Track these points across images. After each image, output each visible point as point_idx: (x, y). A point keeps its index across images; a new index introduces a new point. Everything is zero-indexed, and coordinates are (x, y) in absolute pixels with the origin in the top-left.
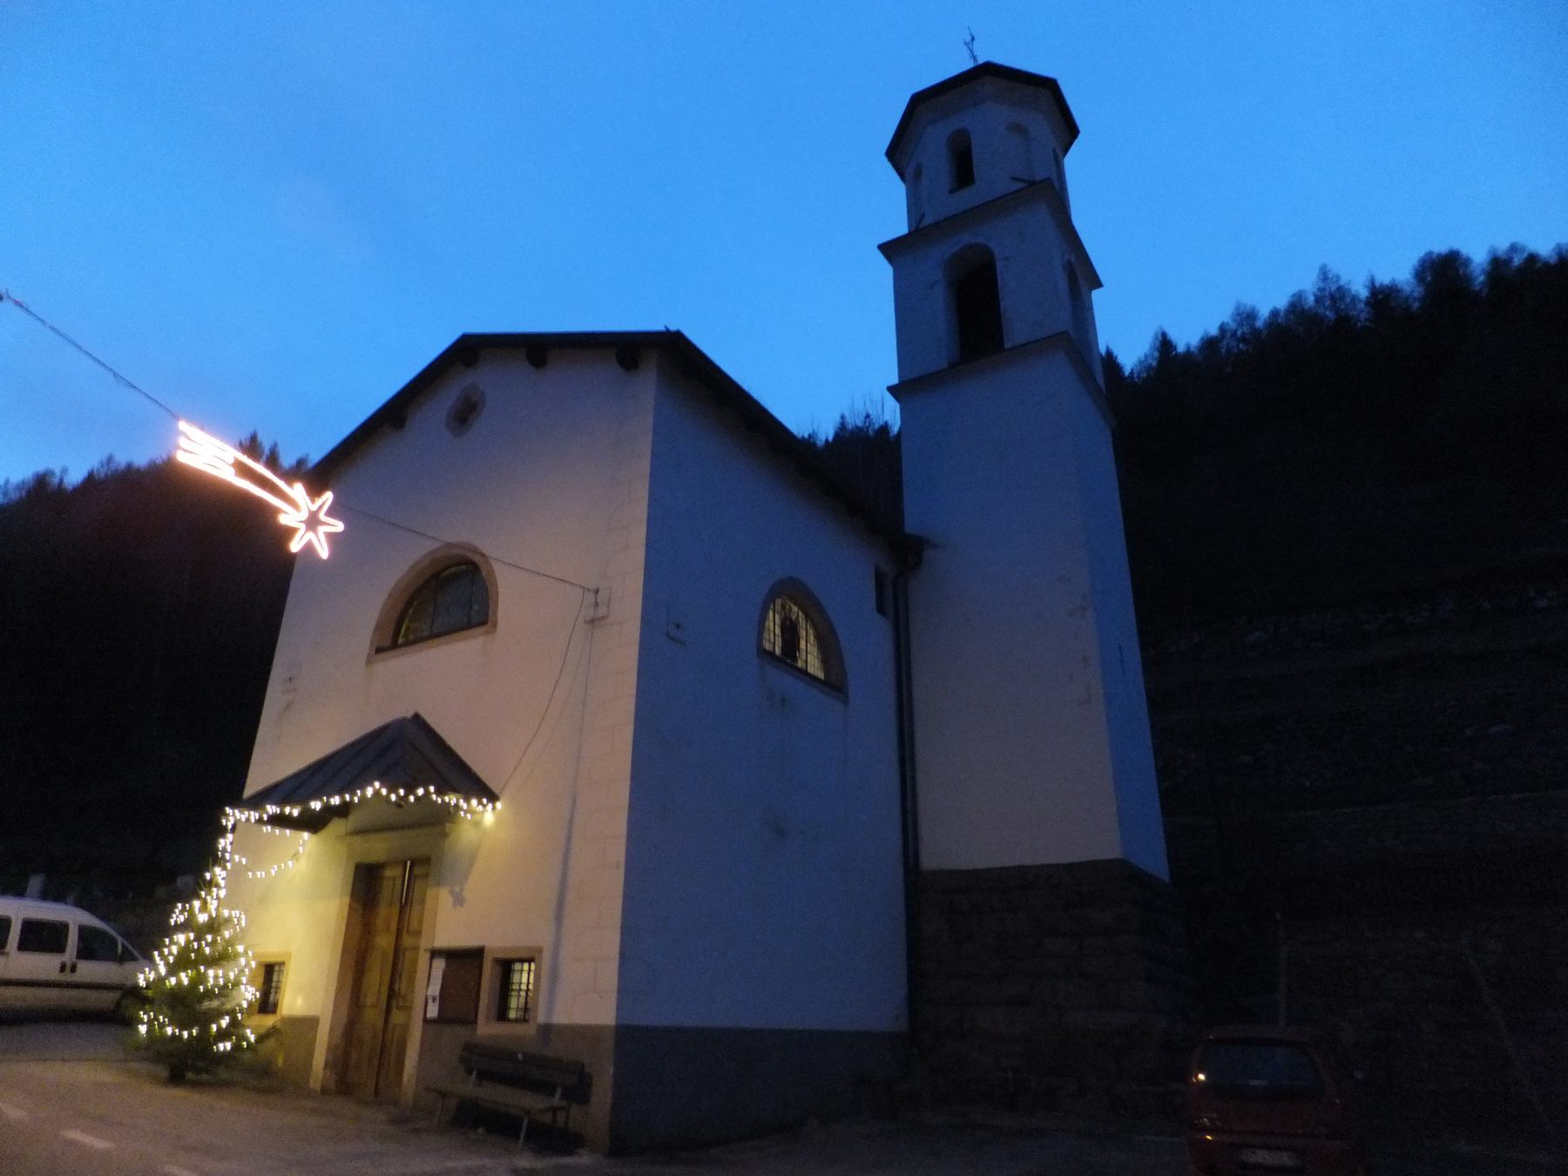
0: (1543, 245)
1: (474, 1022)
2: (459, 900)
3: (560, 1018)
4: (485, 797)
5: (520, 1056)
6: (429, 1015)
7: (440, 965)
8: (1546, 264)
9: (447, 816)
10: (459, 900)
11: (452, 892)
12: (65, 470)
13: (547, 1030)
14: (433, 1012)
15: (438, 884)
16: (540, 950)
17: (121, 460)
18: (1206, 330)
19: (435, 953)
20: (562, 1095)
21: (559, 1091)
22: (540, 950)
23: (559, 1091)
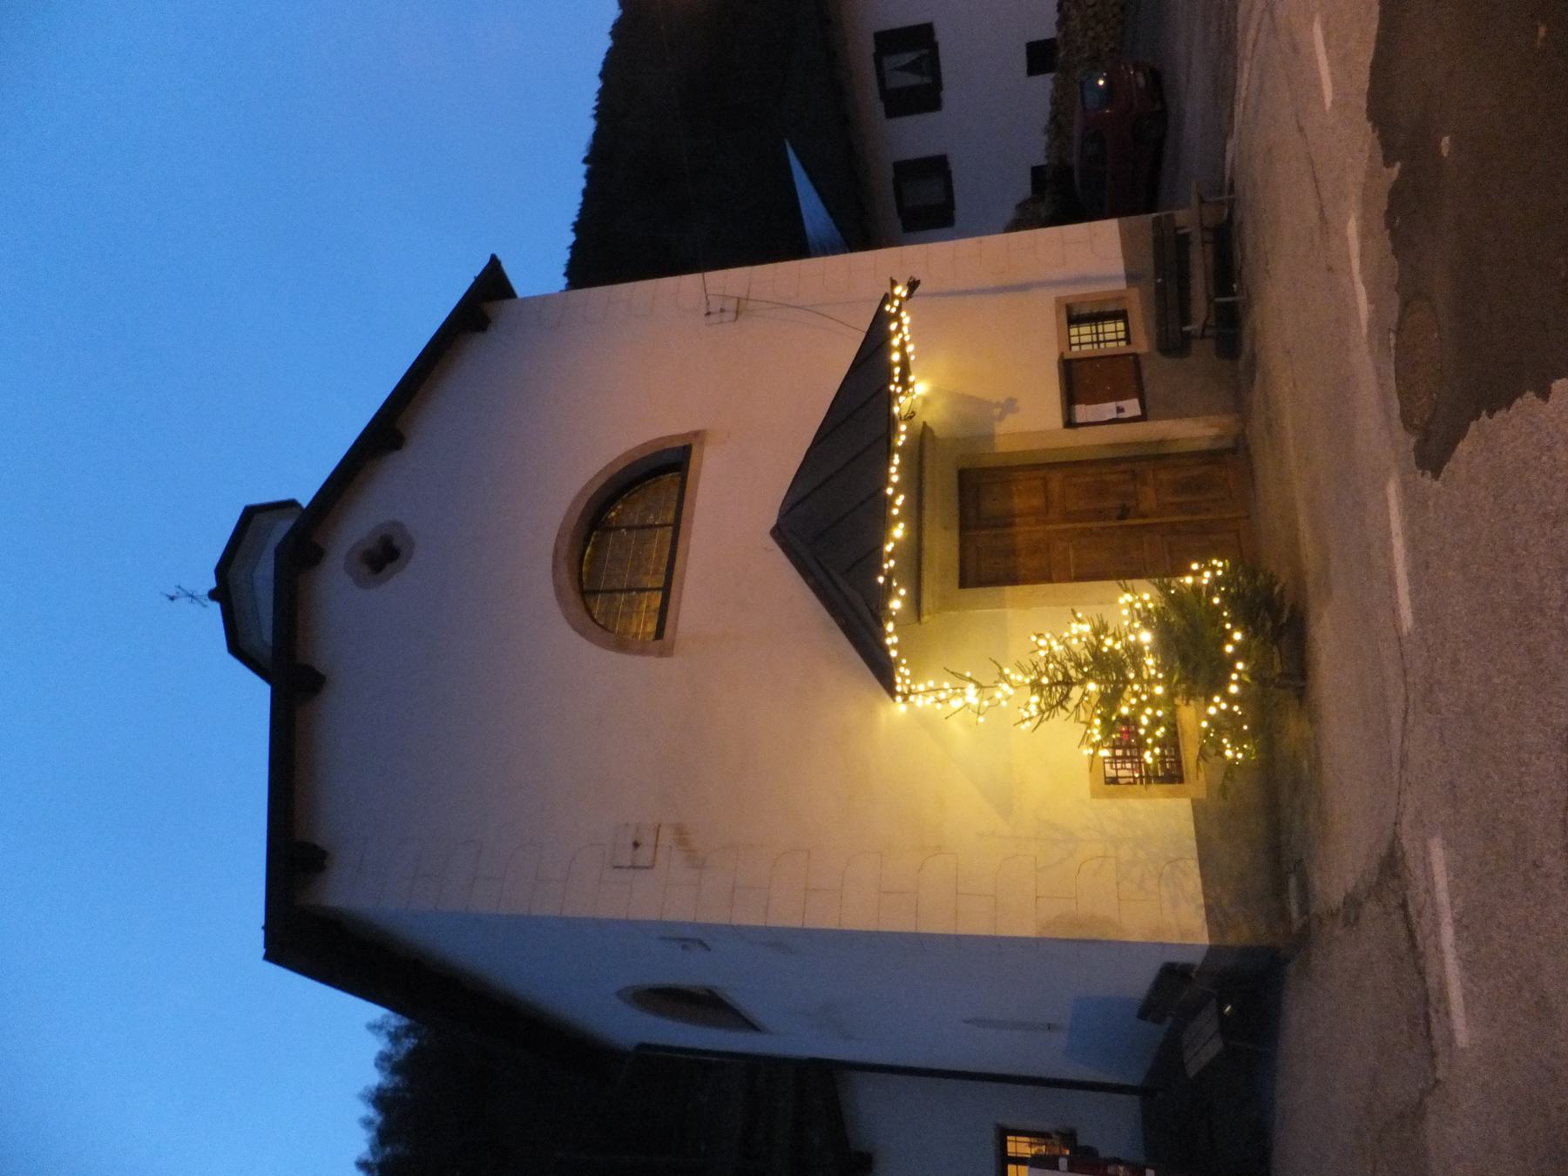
0: (613, 11)
1: (1135, 355)
2: (1010, 406)
3: (1117, 267)
4: (890, 513)
5: (1159, 280)
6: (1137, 412)
7: (1083, 412)
8: (603, 86)
9: (923, 439)
10: (1010, 406)
11: (1001, 418)
12: (374, 1027)
13: (1131, 277)
14: (1132, 407)
15: (990, 437)
16: (1058, 300)
17: (566, 262)
18: (362, 1097)
19: (1070, 423)
20: (1187, 325)
21: (1186, 329)
22: (1058, 300)
23: (1186, 329)
